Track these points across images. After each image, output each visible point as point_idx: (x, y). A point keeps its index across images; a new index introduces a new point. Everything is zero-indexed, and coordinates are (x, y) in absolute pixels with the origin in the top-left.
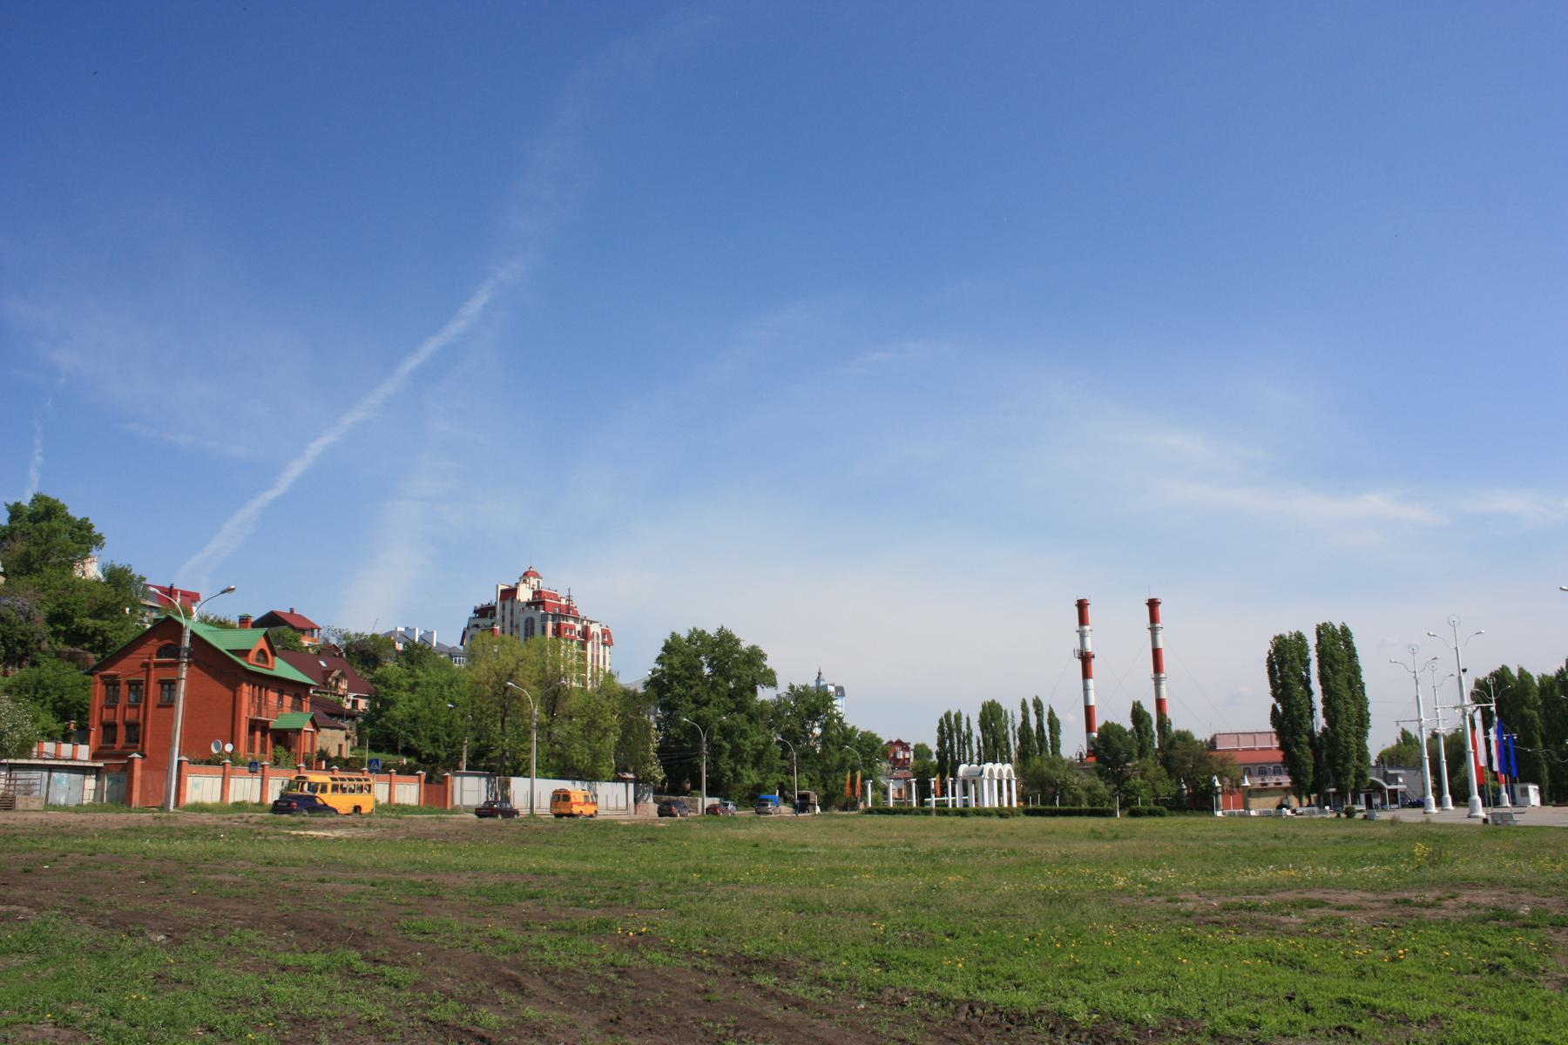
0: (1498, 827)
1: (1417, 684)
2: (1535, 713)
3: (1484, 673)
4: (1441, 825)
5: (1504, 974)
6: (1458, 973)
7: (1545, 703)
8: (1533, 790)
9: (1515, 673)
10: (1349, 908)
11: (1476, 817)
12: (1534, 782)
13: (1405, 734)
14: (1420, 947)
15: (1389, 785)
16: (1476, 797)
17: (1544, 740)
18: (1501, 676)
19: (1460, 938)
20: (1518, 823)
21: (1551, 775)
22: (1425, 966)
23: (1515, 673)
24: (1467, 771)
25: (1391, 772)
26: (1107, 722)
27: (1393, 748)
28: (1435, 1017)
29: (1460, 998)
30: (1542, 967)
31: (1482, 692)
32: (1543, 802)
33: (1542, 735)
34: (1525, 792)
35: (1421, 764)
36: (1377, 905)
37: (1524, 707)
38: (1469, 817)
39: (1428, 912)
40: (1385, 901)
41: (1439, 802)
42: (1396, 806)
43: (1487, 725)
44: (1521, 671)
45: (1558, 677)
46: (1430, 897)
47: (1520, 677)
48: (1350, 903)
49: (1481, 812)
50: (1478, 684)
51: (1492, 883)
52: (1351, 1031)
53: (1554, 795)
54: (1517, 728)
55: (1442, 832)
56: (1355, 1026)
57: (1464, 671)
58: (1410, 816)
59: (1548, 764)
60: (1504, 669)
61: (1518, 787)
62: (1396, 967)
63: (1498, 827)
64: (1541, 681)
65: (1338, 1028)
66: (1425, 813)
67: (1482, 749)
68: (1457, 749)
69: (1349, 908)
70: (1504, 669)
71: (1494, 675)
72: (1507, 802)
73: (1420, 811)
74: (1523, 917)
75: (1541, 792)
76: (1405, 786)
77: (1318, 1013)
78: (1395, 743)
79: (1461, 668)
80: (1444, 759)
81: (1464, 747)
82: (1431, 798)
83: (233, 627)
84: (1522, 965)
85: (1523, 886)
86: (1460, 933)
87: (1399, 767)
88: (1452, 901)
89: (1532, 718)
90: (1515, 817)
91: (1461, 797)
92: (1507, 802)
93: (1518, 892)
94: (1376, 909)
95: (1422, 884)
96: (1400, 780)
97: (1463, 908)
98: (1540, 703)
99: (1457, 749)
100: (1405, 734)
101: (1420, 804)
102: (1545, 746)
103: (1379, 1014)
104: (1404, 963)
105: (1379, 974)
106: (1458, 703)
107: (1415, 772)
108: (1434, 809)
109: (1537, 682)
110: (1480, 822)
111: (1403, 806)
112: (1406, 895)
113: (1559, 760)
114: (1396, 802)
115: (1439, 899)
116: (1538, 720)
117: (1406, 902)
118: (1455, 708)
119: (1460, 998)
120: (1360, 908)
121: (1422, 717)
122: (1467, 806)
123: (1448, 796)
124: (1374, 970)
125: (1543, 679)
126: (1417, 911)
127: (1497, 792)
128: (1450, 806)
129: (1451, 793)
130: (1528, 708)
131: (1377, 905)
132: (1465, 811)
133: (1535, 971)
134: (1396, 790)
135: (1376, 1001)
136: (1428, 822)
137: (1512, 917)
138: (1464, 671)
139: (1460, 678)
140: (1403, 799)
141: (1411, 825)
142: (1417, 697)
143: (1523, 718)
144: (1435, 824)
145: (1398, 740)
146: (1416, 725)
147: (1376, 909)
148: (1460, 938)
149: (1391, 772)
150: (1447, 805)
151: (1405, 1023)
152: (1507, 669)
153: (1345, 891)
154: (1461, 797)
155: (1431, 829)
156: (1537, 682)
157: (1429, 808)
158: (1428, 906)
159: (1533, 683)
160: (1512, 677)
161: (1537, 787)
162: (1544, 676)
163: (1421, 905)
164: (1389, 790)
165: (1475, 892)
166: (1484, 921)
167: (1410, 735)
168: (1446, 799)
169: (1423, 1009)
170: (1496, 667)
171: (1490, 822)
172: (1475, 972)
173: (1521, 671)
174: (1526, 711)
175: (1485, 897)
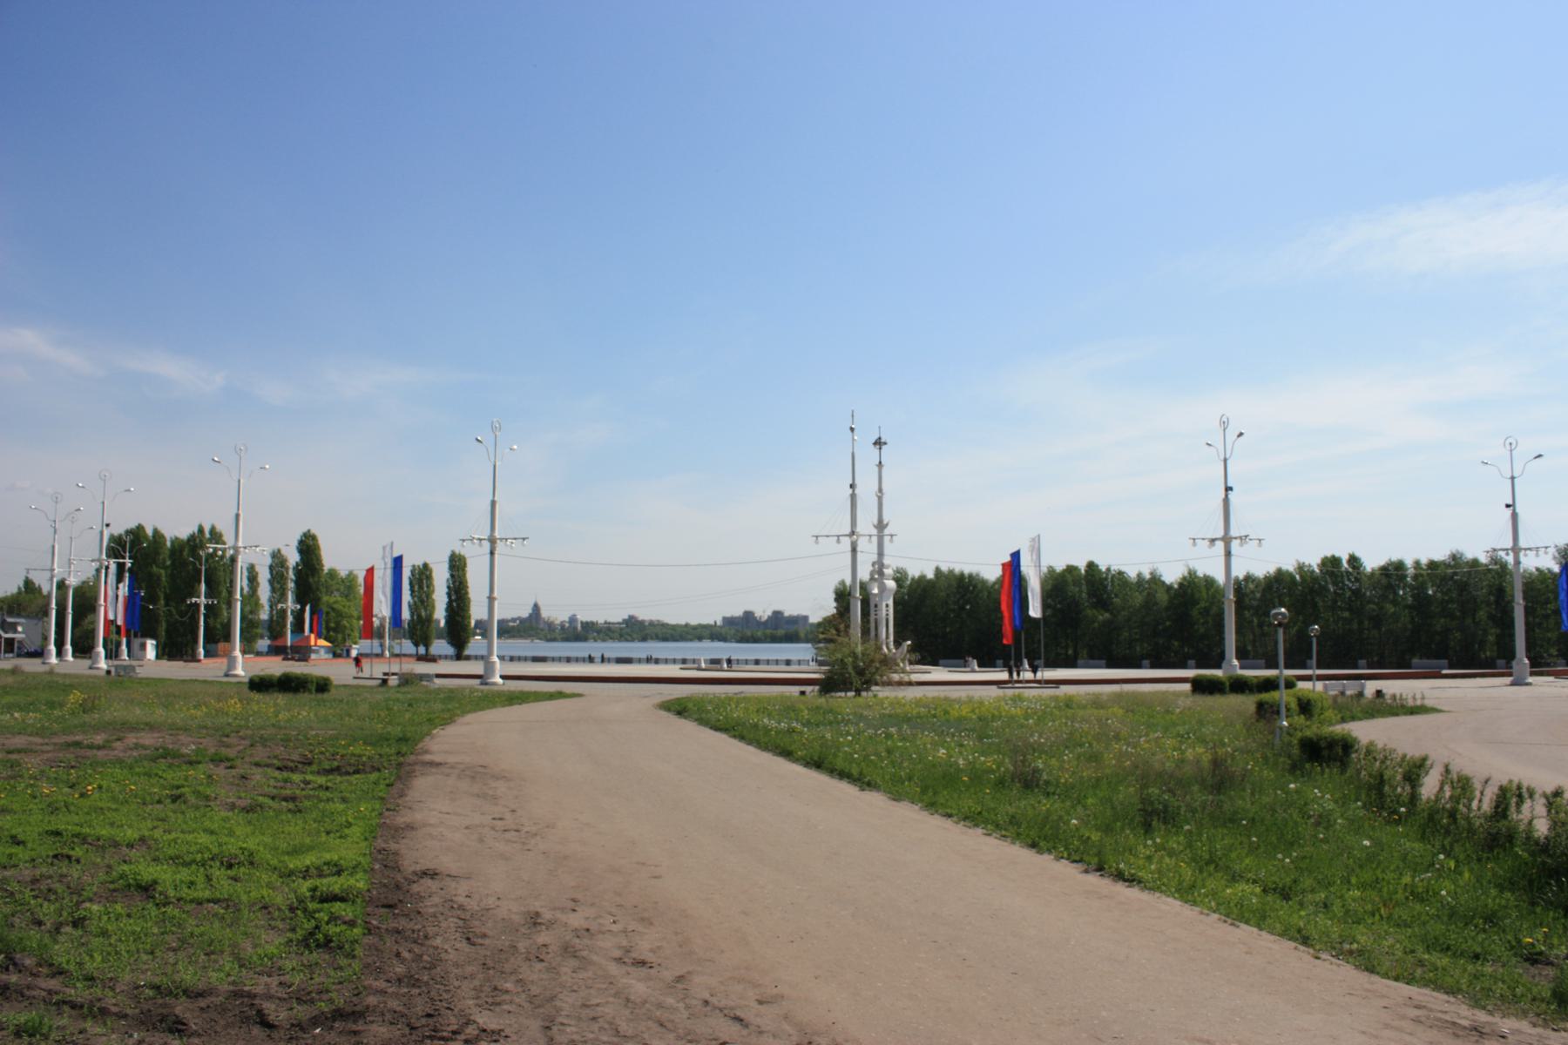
0: (120, 679)
1: (55, 532)
2: (163, 572)
3: (119, 529)
4: (65, 675)
5: (185, 802)
6: (144, 804)
7: (173, 564)
8: (150, 645)
9: (149, 532)
10: (19, 751)
11: (98, 668)
12: (152, 637)
13: (28, 584)
14: (104, 784)
15: (6, 632)
16: (101, 650)
17: (167, 599)
18: (137, 534)
19: (139, 775)
20: (140, 676)
21: (167, 631)
22: (114, 799)
23: (149, 532)
24: (94, 622)
25: (10, 620)
26: (309, 531)
27: (13, 595)
28: (142, 840)
29: (156, 823)
30: (213, 795)
31: (117, 547)
32: (158, 657)
33: (165, 593)
34: (143, 647)
35: (46, 613)
36: (49, 748)
37: (154, 567)
38: (91, 668)
39: (100, 753)
40: (55, 744)
41: (60, 653)
42: (11, 655)
43: (120, 579)
44: (156, 531)
45: (189, 540)
46: (99, 739)
47: (154, 537)
48: (19, 746)
49: (103, 664)
50: (113, 539)
51: (151, 727)
52: (69, 857)
53: (167, 650)
54: (143, 585)
55: (68, 682)
56: (71, 853)
57: (108, 525)
58: (31, 665)
59: (168, 621)
60: (140, 528)
61: (136, 642)
62: (85, 803)
63: (120, 679)
64: (172, 542)
65: (55, 856)
66: (44, 663)
67: (112, 606)
68: (86, 601)
69: (19, 751)
70: (140, 528)
71: (128, 532)
72: (125, 656)
73: (38, 661)
74: (188, 755)
75: (157, 647)
76: (23, 636)
77: (30, 845)
78: (15, 591)
79: (105, 522)
80: (70, 610)
81: (96, 599)
82: (53, 648)
83: (1514, 511)
84: (197, 793)
85: (178, 729)
86: (137, 770)
87: (19, 615)
88: (118, 743)
89: (159, 578)
90: (138, 670)
91: (84, 648)
92: (125, 656)
93: (178, 734)
94: (48, 752)
95: (85, 729)
96: (20, 629)
97: (131, 749)
98: (168, 563)
99: (86, 601)
100: (28, 584)
101: (40, 653)
102: (167, 605)
103: (90, 841)
104: (92, 798)
105: (72, 808)
106: (96, 557)
107: (35, 622)
108: (54, 660)
109: (168, 544)
110: (103, 673)
111: (19, 656)
112: (78, 738)
113: (177, 617)
114: (12, 651)
115: (108, 741)
116: (164, 579)
117: (77, 744)
118: (93, 561)
119: (156, 823)
120: (31, 751)
121: (56, 566)
122: (90, 658)
123: (69, 647)
124: (66, 807)
125: (175, 541)
126: (89, 753)
127: (119, 644)
128: (70, 658)
129: (72, 645)
130: (158, 566)
131: (49, 748)
132: (87, 662)
133: (207, 798)
134: (13, 639)
135: (86, 830)
136: (51, 672)
137: (176, 755)
138: (108, 525)
139: (102, 533)
140: (19, 648)
141: (35, 675)
142: (53, 547)
143: (151, 575)
144: (58, 674)
145: (19, 588)
146: (48, 574)
147: (48, 752)
148: (139, 775)
149: (10, 620)
150: (66, 655)
151: (115, 847)
152: (143, 527)
153: (9, 736)
154: (84, 648)
155: (55, 679)
156: (168, 544)
157: (49, 658)
158: (99, 748)
159: (165, 544)
160: (146, 536)
161: (154, 642)
162: (177, 538)
163: (91, 747)
164: (6, 639)
165: (139, 735)
166: (154, 760)
167: (33, 583)
168: (67, 650)
169: (131, 834)
170: (132, 525)
171: (113, 673)
172: (159, 802)
173: (156, 531)
174: (155, 569)
175: (148, 739)
